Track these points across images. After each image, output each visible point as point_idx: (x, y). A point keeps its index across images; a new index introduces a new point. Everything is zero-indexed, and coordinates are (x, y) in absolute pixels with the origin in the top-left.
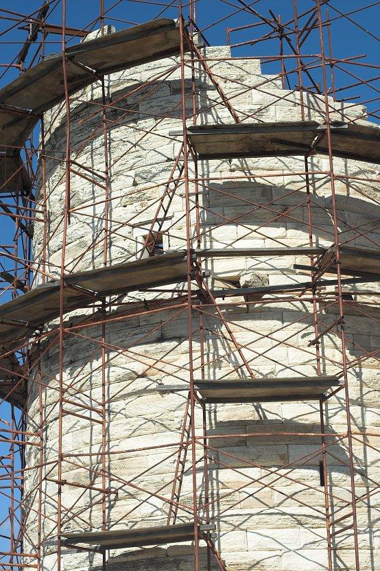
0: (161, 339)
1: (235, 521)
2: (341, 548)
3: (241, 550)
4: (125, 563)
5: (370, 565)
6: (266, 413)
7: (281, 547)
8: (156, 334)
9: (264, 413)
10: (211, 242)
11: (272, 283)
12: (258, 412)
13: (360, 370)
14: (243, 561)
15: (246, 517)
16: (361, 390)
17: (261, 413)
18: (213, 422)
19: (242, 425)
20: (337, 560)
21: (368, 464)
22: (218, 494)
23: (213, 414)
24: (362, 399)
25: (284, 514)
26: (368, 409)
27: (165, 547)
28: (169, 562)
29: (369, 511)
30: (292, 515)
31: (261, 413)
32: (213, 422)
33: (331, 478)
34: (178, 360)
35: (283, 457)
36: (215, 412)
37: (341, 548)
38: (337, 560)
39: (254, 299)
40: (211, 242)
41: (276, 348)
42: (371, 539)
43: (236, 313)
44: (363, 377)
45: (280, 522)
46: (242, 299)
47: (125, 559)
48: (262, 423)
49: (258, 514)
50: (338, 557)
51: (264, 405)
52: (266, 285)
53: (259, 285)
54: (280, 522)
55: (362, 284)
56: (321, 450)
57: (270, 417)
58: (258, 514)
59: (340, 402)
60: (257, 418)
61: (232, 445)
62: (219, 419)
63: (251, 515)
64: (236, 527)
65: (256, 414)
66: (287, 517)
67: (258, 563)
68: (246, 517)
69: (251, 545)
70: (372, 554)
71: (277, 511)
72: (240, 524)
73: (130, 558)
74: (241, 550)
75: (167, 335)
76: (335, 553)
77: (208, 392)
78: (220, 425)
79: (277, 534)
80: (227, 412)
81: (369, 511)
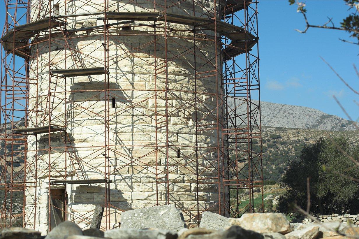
0: (57, 49)
1: (79, 122)
2: (119, 133)
3: (80, 134)
4: (45, 139)
5: (131, 139)
6: (92, 79)
7: (95, 133)
8: (55, 47)
9: (91, 79)
10: (75, 7)
11: (98, 25)
12: (89, 78)
13: (134, 59)
14: (80, 138)
15: (83, 121)
16: (133, 67)
17: (90, 79)
18: (73, 83)
19: (83, 84)
20: (117, 137)
21: (134, 98)
22: (73, 112)
23: (72, 80)
24: (133, 71)
25: (96, 119)
26: (135, 75)
27: (56, 133)
28: (57, 139)
29: (132, 118)
30: (99, 120)
31: (90, 79)
32: (73, 83)
33: (116, 105)
34: (62, 59)
35: (97, 97)
36: (74, 79)
37: (119, 133)
38: (117, 137)
39: (89, 32)
40: (75, 7)
41: (92, 52)
42: (132, 128)
43: (82, 38)
44: (134, 61)
45: (95, 123)
46: (85, 32)
47: (44, 137)
48: (91, 83)
49: (87, 120)
50: (118, 136)
51: (91, 76)
52: (94, 25)
53: (90, 26)
54: (95, 123)
55: (137, 21)
56: (111, 93)
57: (94, 80)
58: (87, 120)
59: (123, 73)
60: (89, 81)
61: (80, 92)
62: (75, 82)
63: (84, 120)
64: (79, 125)
65: (88, 79)
66: (97, 121)
67: (86, 139)
68: (83, 121)
69: (84, 132)
70: (132, 134)
71: (94, 118)
72: (81, 124)
73: (46, 137)
74: (80, 134)
75: (59, 47)
76: (117, 135)
77: (67, 73)
78: (75, 84)
79: (94, 127)
80: (79, 79)
81: (132, 118)
